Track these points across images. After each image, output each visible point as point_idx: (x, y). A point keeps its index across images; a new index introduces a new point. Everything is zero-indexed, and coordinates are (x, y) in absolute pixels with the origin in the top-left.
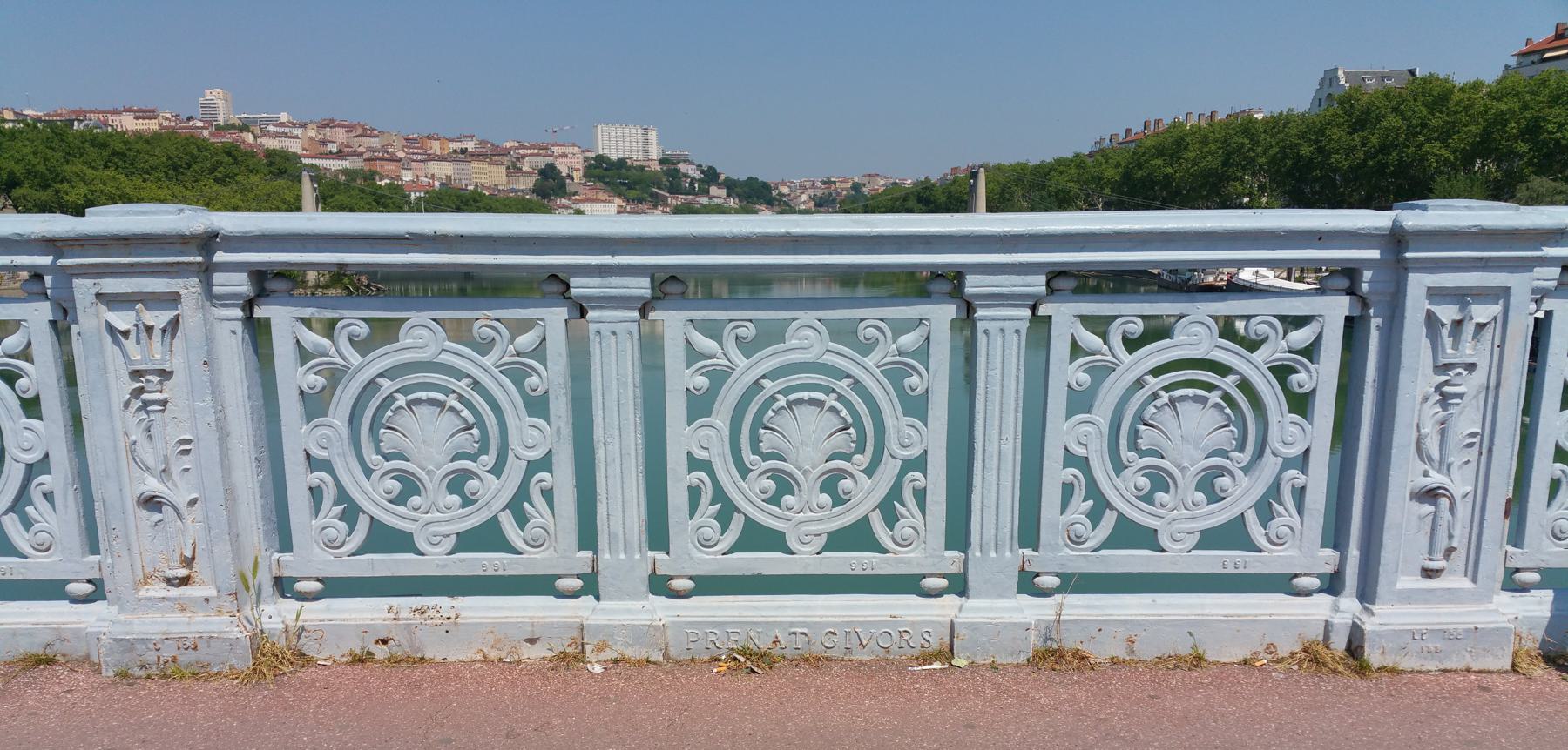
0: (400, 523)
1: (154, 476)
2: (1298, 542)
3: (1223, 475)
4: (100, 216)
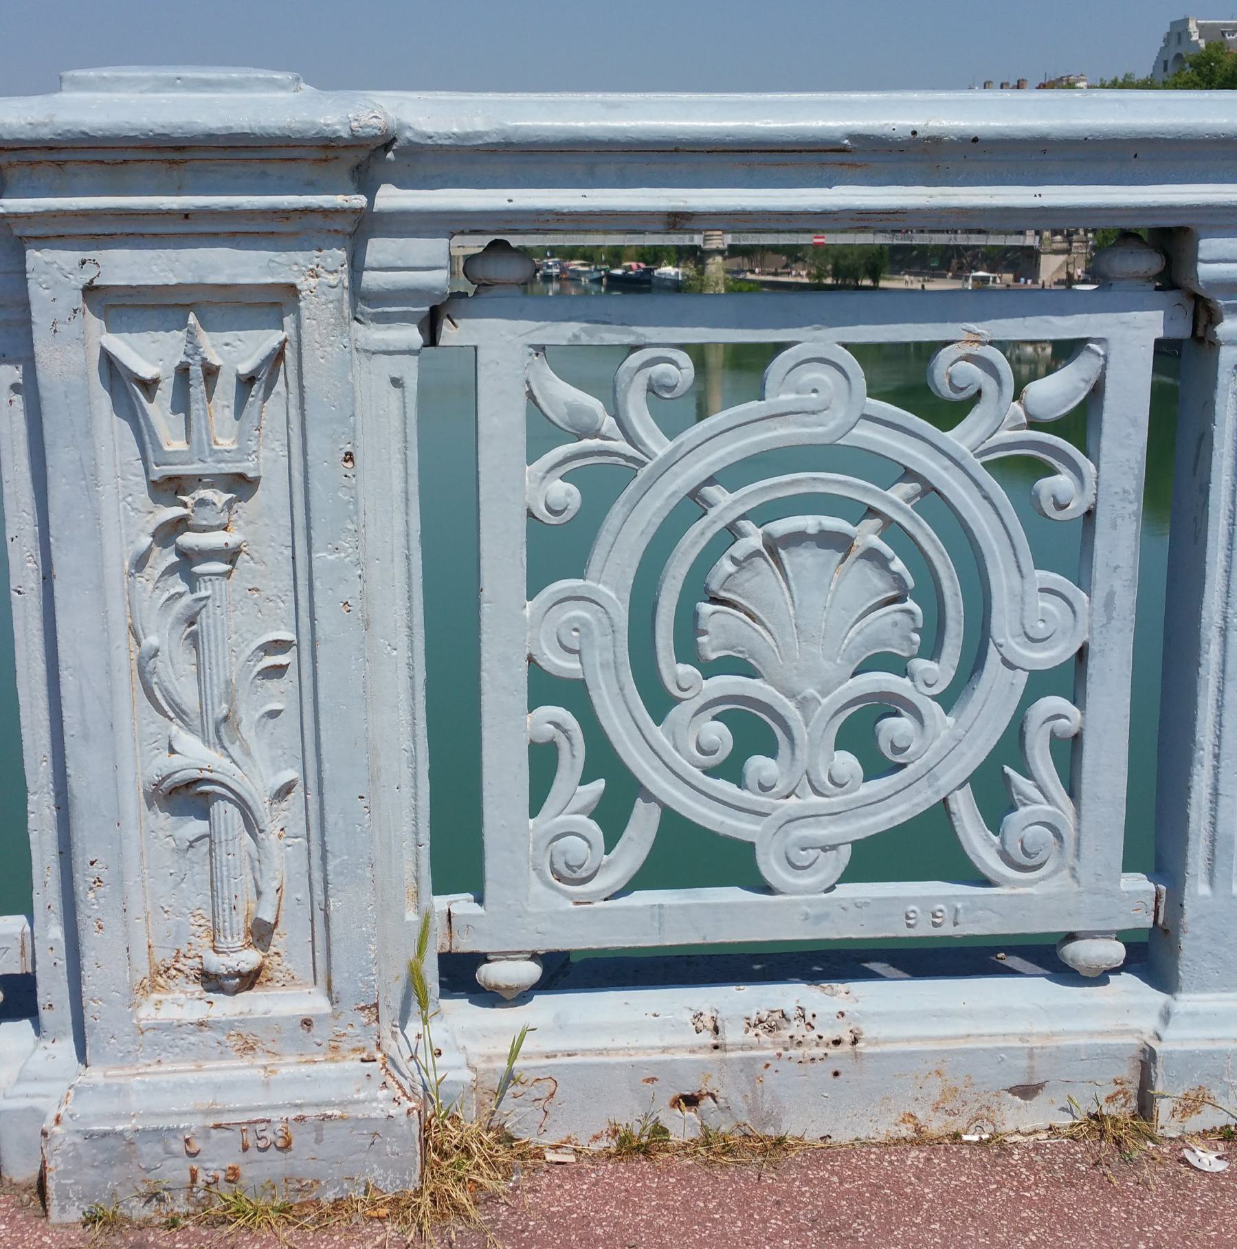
0: (729, 821)
1: (193, 732)
2: (1071, 860)
3: (897, 714)
4: (98, 89)
